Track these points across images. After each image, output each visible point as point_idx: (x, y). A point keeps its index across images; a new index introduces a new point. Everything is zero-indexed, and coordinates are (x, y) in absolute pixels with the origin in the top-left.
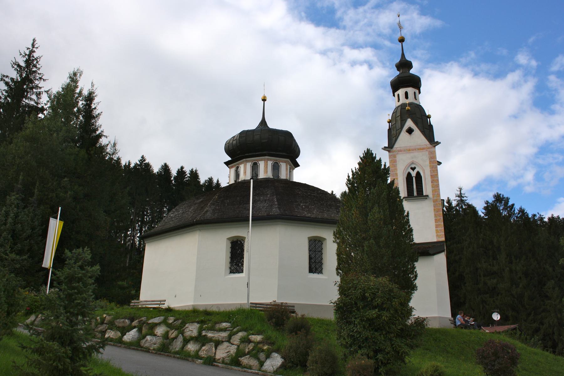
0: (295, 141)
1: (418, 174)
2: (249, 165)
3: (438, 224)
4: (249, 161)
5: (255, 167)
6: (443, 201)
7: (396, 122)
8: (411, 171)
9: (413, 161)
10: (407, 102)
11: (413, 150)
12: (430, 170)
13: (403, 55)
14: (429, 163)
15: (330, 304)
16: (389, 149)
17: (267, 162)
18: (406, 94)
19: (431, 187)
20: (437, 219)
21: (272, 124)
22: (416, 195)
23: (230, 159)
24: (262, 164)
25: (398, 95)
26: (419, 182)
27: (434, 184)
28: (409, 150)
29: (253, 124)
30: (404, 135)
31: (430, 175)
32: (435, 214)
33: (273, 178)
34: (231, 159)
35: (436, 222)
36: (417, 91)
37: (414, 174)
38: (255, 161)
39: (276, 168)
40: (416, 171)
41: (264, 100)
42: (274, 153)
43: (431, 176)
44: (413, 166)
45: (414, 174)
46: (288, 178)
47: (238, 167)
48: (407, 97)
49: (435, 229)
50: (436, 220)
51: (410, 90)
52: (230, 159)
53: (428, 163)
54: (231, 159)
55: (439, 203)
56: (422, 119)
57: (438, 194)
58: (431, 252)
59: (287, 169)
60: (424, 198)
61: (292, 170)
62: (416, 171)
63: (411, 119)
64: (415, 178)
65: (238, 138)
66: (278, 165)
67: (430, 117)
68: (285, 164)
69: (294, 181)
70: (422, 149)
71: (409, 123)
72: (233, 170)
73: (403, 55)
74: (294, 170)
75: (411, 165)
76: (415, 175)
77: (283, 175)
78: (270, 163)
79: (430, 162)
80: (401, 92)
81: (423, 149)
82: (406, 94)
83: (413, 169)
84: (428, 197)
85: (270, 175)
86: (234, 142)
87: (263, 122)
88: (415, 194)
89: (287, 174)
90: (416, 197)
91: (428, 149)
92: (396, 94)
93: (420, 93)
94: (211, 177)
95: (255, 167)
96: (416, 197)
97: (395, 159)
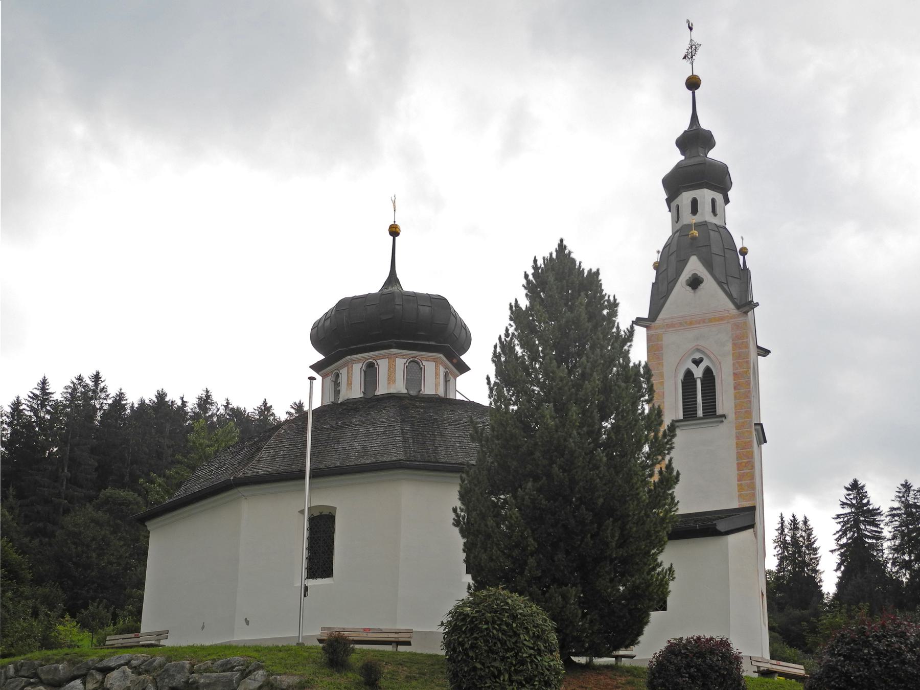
0: (455, 315)
1: (708, 372)
2: (357, 370)
3: (744, 472)
4: (357, 361)
5: (371, 371)
6: (759, 427)
7: (668, 266)
8: (693, 368)
9: (698, 345)
10: (694, 221)
11: (699, 323)
12: (734, 364)
13: (694, 117)
14: (731, 348)
15: (438, 631)
16: (648, 323)
17: (394, 361)
18: (694, 203)
19: (733, 397)
20: (742, 463)
21: (410, 283)
22: (702, 416)
23: (320, 357)
24: (383, 365)
25: (678, 207)
26: (688, 386)
27: (739, 392)
28: (691, 323)
29: (373, 284)
30: (681, 288)
31: (732, 373)
32: (737, 452)
33: (408, 393)
34: (324, 357)
35: (738, 470)
36: (719, 197)
37: (698, 372)
38: (370, 359)
39: (414, 373)
40: (702, 366)
41: (394, 231)
42: (427, 343)
43: (735, 374)
44: (697, 356)
45: (698, 372)
46: (441, 393)
47: (337, 376)
48: (694, 210)
49: (737, 483)
50: (739, 465)
51: (706, 195)
52: (320, 357)
53: (729, 347)
54: (324, 357)
55: (747, 431)
56: (725, 257)
57: (746, 412)
58: (721, 526)
59: (437, 374)
60: (717, 422)
61: (451, 378)
62: (702, 366)
63: (697, 256)
64: (701, 381)
65: (333, 313)
66: (419, 365)
67: (746, 253)
68: (434, 363)
69: (457, 399)
70: (718, 321)
71: (694, 266)
72: (329, 379)
73: (694, 117)
74: (458, 378)
75: (693, 353)
76: (701, 375)
77: (430, 387)
78: (400, 363)
79: (734, 344)
80: (685, 198)
81: (722, 319)
82: (694, 203)
83: (697, 362)
84: (726, 418)
85: (400, 387)
86: (328, 322)
87: (393, 279)
88: (700, 413)
89: (437, 385)
90: (700, 419)
91: (731, 318)
92: (673, 204)
93: (727, 201)
94: (97, 378)
95: (371, 371)
96: (700, 419)
97: (660, 343)
